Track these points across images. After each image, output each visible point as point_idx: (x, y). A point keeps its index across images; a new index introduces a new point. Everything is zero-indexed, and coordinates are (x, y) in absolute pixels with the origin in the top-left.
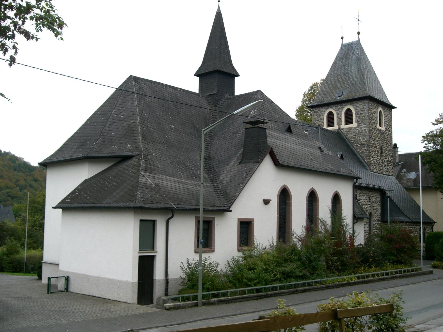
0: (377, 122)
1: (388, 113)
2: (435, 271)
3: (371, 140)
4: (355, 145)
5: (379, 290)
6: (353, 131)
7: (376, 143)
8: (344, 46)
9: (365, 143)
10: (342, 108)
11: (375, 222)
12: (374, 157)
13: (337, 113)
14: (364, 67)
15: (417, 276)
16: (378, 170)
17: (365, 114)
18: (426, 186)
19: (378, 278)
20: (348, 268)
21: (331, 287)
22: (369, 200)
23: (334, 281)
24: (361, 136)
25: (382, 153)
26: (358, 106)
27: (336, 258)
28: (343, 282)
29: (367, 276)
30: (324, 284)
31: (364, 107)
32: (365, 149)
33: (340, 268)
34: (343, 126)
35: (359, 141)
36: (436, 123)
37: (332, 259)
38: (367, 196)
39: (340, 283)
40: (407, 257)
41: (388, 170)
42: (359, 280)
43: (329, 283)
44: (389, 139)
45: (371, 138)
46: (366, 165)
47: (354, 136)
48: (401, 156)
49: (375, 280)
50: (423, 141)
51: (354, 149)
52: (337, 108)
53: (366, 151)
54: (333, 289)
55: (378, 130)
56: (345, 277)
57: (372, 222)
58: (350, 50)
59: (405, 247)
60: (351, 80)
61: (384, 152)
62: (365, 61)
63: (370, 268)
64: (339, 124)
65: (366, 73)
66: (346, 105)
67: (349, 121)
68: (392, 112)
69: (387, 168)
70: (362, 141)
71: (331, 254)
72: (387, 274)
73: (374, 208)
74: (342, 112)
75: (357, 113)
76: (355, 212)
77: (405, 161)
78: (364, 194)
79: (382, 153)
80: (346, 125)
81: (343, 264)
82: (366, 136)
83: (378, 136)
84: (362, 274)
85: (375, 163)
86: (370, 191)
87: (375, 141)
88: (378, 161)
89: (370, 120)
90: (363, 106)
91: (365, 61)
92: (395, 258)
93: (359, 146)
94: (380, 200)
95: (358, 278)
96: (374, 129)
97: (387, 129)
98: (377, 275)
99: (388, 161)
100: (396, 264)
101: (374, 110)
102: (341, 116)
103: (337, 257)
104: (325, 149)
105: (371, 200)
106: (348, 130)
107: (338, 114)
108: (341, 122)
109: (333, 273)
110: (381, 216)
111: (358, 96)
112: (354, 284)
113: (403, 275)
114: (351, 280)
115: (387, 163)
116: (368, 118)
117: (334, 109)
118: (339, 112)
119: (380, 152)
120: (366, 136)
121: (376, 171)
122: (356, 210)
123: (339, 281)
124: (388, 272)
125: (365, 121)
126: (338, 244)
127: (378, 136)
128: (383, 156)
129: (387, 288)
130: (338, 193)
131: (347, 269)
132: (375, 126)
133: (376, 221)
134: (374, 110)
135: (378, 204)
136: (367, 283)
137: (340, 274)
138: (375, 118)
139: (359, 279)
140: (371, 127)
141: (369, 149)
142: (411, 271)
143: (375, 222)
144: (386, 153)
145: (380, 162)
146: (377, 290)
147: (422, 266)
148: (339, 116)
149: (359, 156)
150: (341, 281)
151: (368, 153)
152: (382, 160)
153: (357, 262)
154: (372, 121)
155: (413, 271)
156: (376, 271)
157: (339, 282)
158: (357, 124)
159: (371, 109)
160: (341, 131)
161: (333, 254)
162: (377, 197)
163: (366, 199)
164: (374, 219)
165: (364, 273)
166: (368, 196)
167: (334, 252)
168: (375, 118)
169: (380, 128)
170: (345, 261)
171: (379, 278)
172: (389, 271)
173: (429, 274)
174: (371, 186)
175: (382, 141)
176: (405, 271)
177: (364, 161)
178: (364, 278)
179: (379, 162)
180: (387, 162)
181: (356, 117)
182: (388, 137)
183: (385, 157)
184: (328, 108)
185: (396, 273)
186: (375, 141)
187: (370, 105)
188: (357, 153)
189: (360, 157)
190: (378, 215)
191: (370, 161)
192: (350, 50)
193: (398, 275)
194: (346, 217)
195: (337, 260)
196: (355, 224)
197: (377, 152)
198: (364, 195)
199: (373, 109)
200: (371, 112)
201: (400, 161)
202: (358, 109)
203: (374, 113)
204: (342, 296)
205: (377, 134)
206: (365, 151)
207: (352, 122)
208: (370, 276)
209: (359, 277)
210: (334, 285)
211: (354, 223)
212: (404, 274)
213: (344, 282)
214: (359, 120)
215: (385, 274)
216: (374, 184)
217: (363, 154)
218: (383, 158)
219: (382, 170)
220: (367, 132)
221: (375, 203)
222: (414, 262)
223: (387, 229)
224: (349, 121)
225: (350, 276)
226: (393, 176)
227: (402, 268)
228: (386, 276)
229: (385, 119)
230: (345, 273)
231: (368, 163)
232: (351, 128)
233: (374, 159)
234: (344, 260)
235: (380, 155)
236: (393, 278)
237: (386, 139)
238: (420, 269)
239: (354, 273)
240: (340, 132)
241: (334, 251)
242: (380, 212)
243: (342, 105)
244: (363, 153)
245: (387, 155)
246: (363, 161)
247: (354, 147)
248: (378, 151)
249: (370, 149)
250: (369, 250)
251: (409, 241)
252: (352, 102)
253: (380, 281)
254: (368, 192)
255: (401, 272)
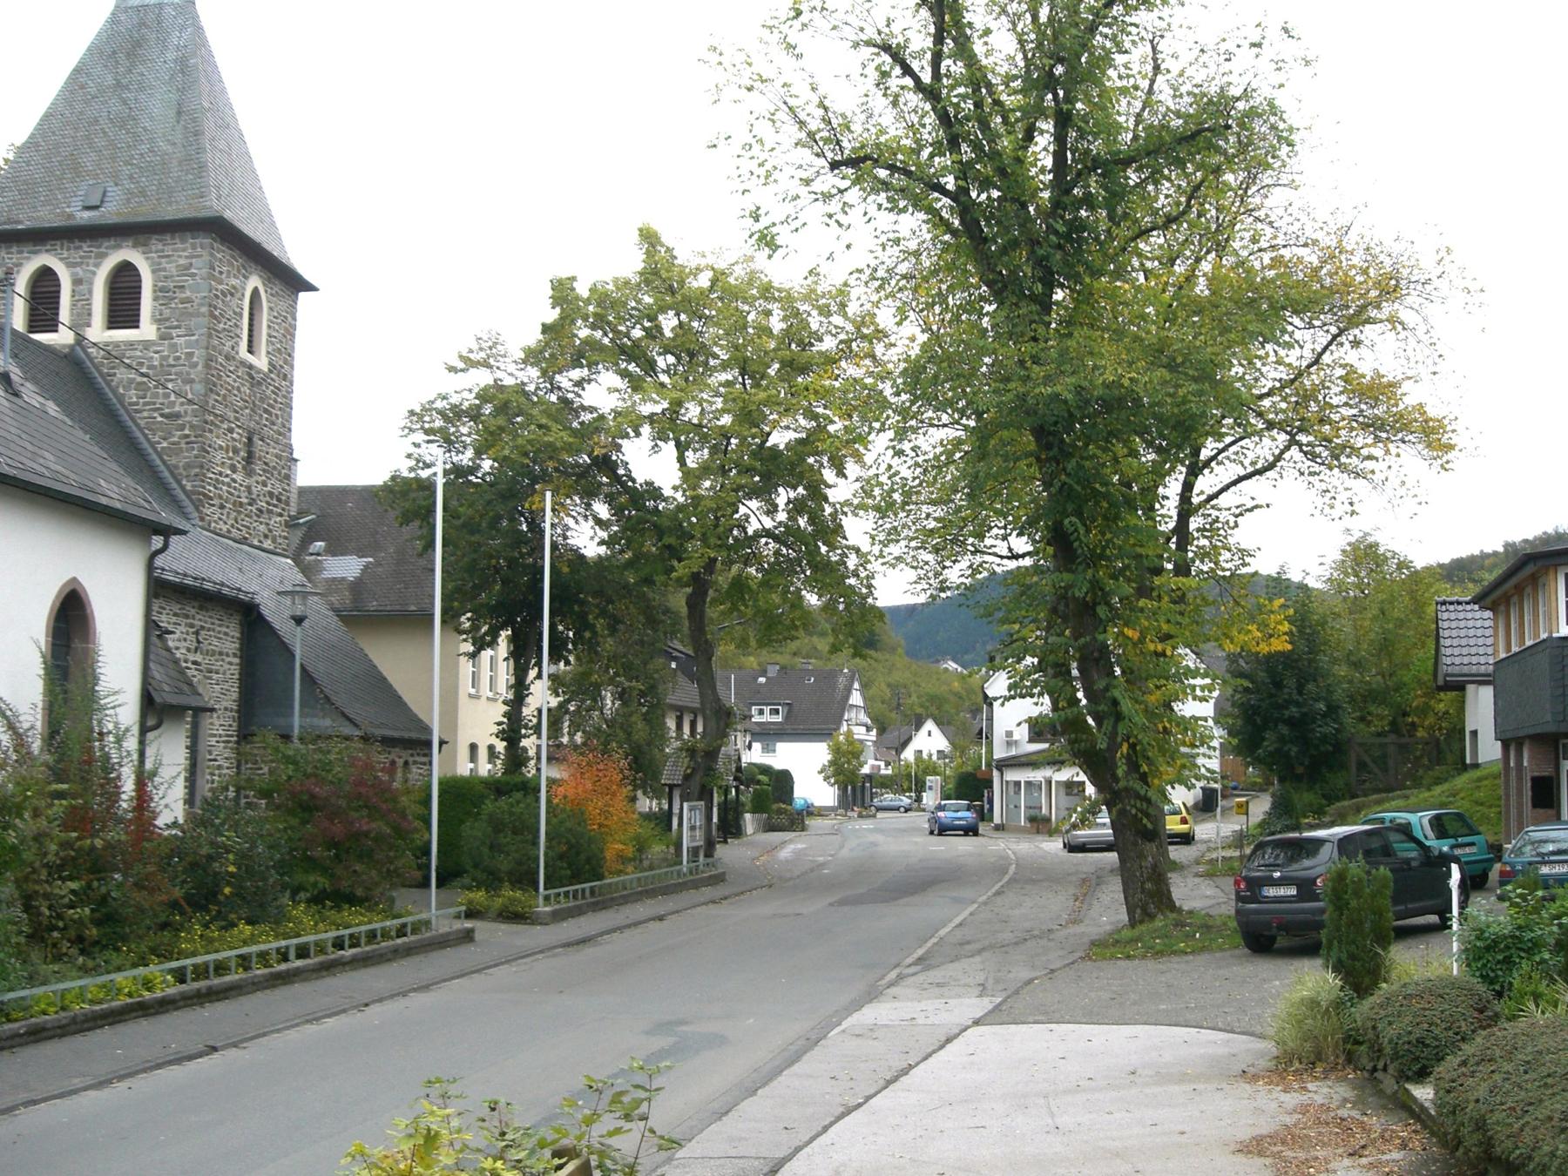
0: (238, 332)
1: (282, 305)
2: (481, 927)
3: (211, 402)
4: (145, 414)
5: (288, 1028)
6: (140, 357)
7: (231, 415)
8: (126, 10)
9: (186, 412)
10: (96, 257)
11: (215, 736)
12: (221, 474)
13: (73, 275)
14: (206, 104)
15: (417, 954)
16: (232, 526)
17: (197, 291)
18: (398, 607)
19: (267, 971)
20: (127, 930)
21: (51, 1033)
22: (195, 644)
23: (69, 996)
24: (171, 380)
25: (250, 458)
26: (168, 256)
27: (74, 885)
28: (112, 1000)
29: (221, 968)
30: (16, 1020)
31: (194, 260)
32: (187, 436)
33: (93, 932)
34: (98, 332)
35: (161, 401)
36: (461, 365)
37: (57, 891)
38: (186, 625)
39: (97, 1008)
40: (374, 873)
41: (270, 531)
42: (184, 987)
43: (45, 1013)
44: (280, 409)
45: (211, 390)
46: (187, 502)
47: (139, 379)
48: (303, 491)
49: (254, 984)
50: (407, 431)
51: (138, 434)
52: (76, 256)
53: (187, 443)
54: (67, 1040)
55: (243, 363)
56: (118, 977)
57: (201, 733)
58: (147, 27)
59: (366, 834)
60: (144, 148)
61: (260, 459)
62: (209, 81)
63: (225, 928)
64: (81, 320)
65: (209, 125)
66: (118, 247)
67: (123, 310)
68: (299, 302)
69: (267, 524)
70: (174, 402)
71: (47, 865)
72: (303, 952)
73: (215, 676)
74: (94, 273)
75: (160, 284)
76: (151, 680)
77: (319, 513)
78: (175, 615)
79: (250, 458)
80: (110, 328)
81: (108, 917)
82: (192, 381)
83: (238, 389)
84: (199, 960)
85: (220, 497)
86: (201, 608)
87: (226, 406)
88: (235, 488)
89: (215, 317)
90: (187, 257)
91: (209, 81)
92: (323, 882)
93: (160, 419)
94: (237, 646)
95: (180, 976)
96: (227, 358)
97: (274, 367)
98: (263, 957)
99: (271, 494)
100: (332, 908)
101: (234, 282)
102: (90, 292)
103: (78, 878)
104: (28, 385)
105: (205, 646)
106: (113, 353)
107: (77, 282)
108: (90, 314)
109: (58, 958)
110: (238, 711)
111: (170, 212)
112: (165, 1005)
113: (368, 952)
114: (149, 989)
115: (268, 503)
116: (204, 309)
117: (61, 259)
118: (81, 273)
119: (242, 453)
120: (192, 381)
121: (225, 528)
122: (157, 673)
123: (89, 996)
124: (307, 943)
125: (193, 322)
126: (79, 820)
127: (238, 389)
128: (255, 474)
129: (317, 1019)
130: (79, 589)
131: (124, 939)
132: (233, 348)
133: (219, 729)
134: (234, 282)
135: (230, 663)
136: (218, 1000)
137: (90, 964)
138: (235, 313)
139: (182, 981)
140: (214, 348)
141: (201, 436)
142: (393, 933)
143: (215, 736)
144: (266, 464)
145: (243, 495)
146: (278, 1031)
147: (434, 911)
148: (84, 287)
149: (158, 462)
150: (101, 995)
151: (195, 452)
152: (249, 488)
153: (174, 905)
154: (222, 325)
155: (401, 932)
156: (252, 940)
157: (92, 1002)
158: (159, 329)
159: (221, 273)
160: (87, 354)
161: (61, 867)
162: (226, 634)
163: (185, 640)
164: (212, 724)
165: (208, 953)
166: (192, 626)
167: (62, 859)
168: (235, 313)
169: (250, 359)
170: (114, 899)
171: (271, 974)
172: (311, 938)
173: (460, 944)
174: (208, 586)
175: (252, 410)
176: (372, 936)
177: (179, 482)
178: (207, 978)
179: (236, 493)
180: (268, 499)
181: (155, 299)
182: (276, 401)
183: (260, 479)
184: (35, 253)
185: (339, 944)
186: (226, 406)
187: (219, 256)
188: (150, 450)
189: (162, 468)
190: (226, 709)
191: (204, 488)
192: (147, 27)
193: (348, 953)
194: (120, 699)
195: (80, 898)
196: (150, 736)
197: (231, 454)
198: (174, 619)
199: (228, 277)
200: (220, 287)
201: (301, 513)
202: (164, 270)
203: (232, 295)
204: (121, 1078)
205: (235, 381)
206: (184, 441)
207: (138, 321)
208: (233, 964)
209: (185, 975)
210: (64, 1022)
211: (144, 730)
212: (368, 948)
213: (114, 1004)
214: (167, 313)
215: (292, 955)
216: (218, 578)
217: (177, 454)
218: (252, 481)
219: (248, 528)
220: (200, 367)
221: (217, 657)
222: (404, 898)
223: (289, 757)
224: (123, 310)
225: (141, 971)
226: (287, 557)
227: (360, 923)
228: (299, 963)
229: (269, 327)
230: (116, 960)
231: (194, 493)
232: (131, 345)
233: (217, 480)
234: (108, 893)
235: (244, 468)
236: (329, 968)
237: (269, 405)
238: (427, 923)
239: (166, 956)
240: (83, 356)
241: (61, 854)
242: (235, 696)
243: (100, 247)
244: (175, 450)
245: (268, 471)
246: (174, 485)
247: (137, 425)
248: (236, 451)
249: (206, 438)
250: (225, 846)
251: (384, 807)
252: (141, 238)
253: (274, 986)
254: (193, 611)
255: (358, 939)
